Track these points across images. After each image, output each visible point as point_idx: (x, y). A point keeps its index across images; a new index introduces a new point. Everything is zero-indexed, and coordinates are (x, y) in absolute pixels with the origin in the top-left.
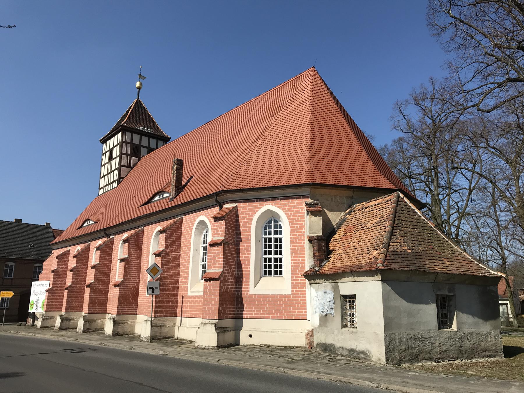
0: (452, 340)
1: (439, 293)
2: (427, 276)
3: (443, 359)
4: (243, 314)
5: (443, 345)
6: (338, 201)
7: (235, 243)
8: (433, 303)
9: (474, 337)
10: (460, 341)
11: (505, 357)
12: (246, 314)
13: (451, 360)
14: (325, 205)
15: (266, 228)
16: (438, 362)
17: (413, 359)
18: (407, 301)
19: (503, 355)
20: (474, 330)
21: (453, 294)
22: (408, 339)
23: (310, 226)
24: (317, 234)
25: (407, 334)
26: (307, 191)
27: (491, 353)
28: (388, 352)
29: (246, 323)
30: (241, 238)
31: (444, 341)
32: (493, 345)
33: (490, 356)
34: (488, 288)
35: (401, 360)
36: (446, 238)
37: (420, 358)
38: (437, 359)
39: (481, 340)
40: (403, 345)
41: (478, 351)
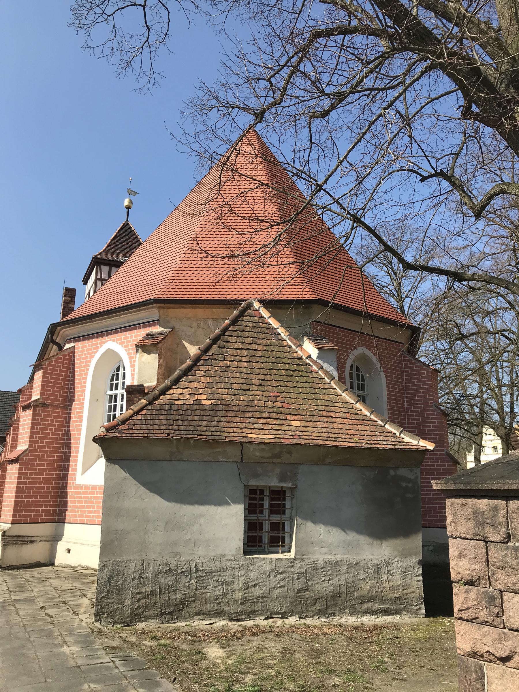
0: (279, 577)
1: (254, 483)
2: (219, 450)
3: (252, 614)
4: (65, 515)
5: (255, 586)
6: (209, 327)
7: (66, 405)
8: (235, 502)
9: (342, 572)
10: (303, 579)
11: (427, 615)
12: (69, 515)
13: (274, 616)
14: (186, 335)
15: (112, 380)
16: (239, 620)
17: (171, 613)
18: (168, 500)
19: (423, 611)
20: (342, 557)
21: (290, 485)
22: (160, 573)
23: (139, 371)
24: (148, 382)
25: (158, 563)
26: (153, 313)
27: (387, 606)
28: (103, 597)
29: (68, 529)
30: (73, 396)
31: (257, 579)
32: (394, 589)
33: (386, 612)
34: (392, 472)
35: (137, 614)
36: (326, 378)
37: (192, 608)
38: (234, 613)
39: (362, 577)
40: (145, 585)
41: (352, 600)
